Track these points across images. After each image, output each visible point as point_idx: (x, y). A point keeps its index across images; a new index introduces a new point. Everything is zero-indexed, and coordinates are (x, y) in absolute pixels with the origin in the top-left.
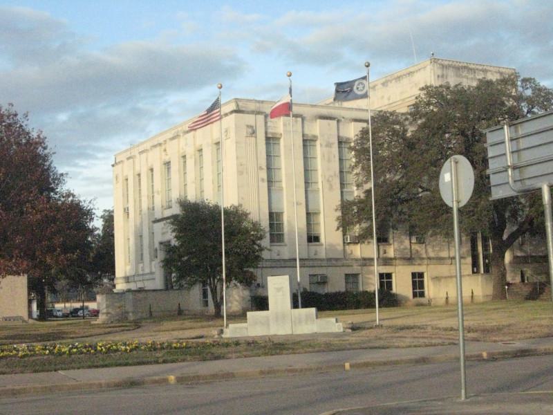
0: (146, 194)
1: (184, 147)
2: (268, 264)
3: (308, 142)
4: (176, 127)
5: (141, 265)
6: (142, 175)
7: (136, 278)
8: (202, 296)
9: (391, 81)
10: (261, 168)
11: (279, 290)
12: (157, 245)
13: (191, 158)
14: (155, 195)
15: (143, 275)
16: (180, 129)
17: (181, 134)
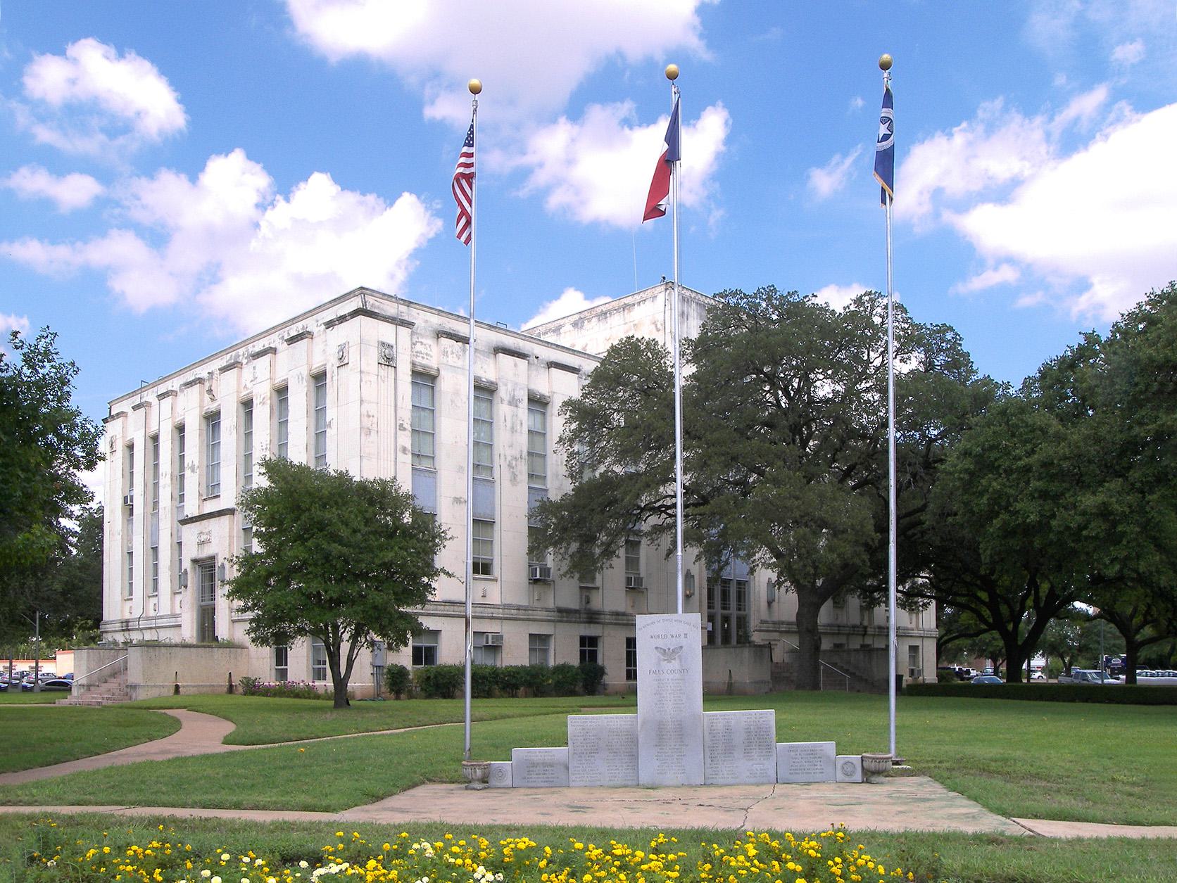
0: (169, 472)
1: (249, 385)
2: (441, 610)
3: (485, 391)
4: (234, 348)
5: (154, 600)
6: (161, 439)
7: (143, 624)
8: (274, 660)
9: (589, 320)
10: (402, 428)
11: (668, 654)
12: (187, 564)
13: (263, 403)
14: (188, 473)
15: (156, 618)
16: (241, 351)
17: (245, 361)
